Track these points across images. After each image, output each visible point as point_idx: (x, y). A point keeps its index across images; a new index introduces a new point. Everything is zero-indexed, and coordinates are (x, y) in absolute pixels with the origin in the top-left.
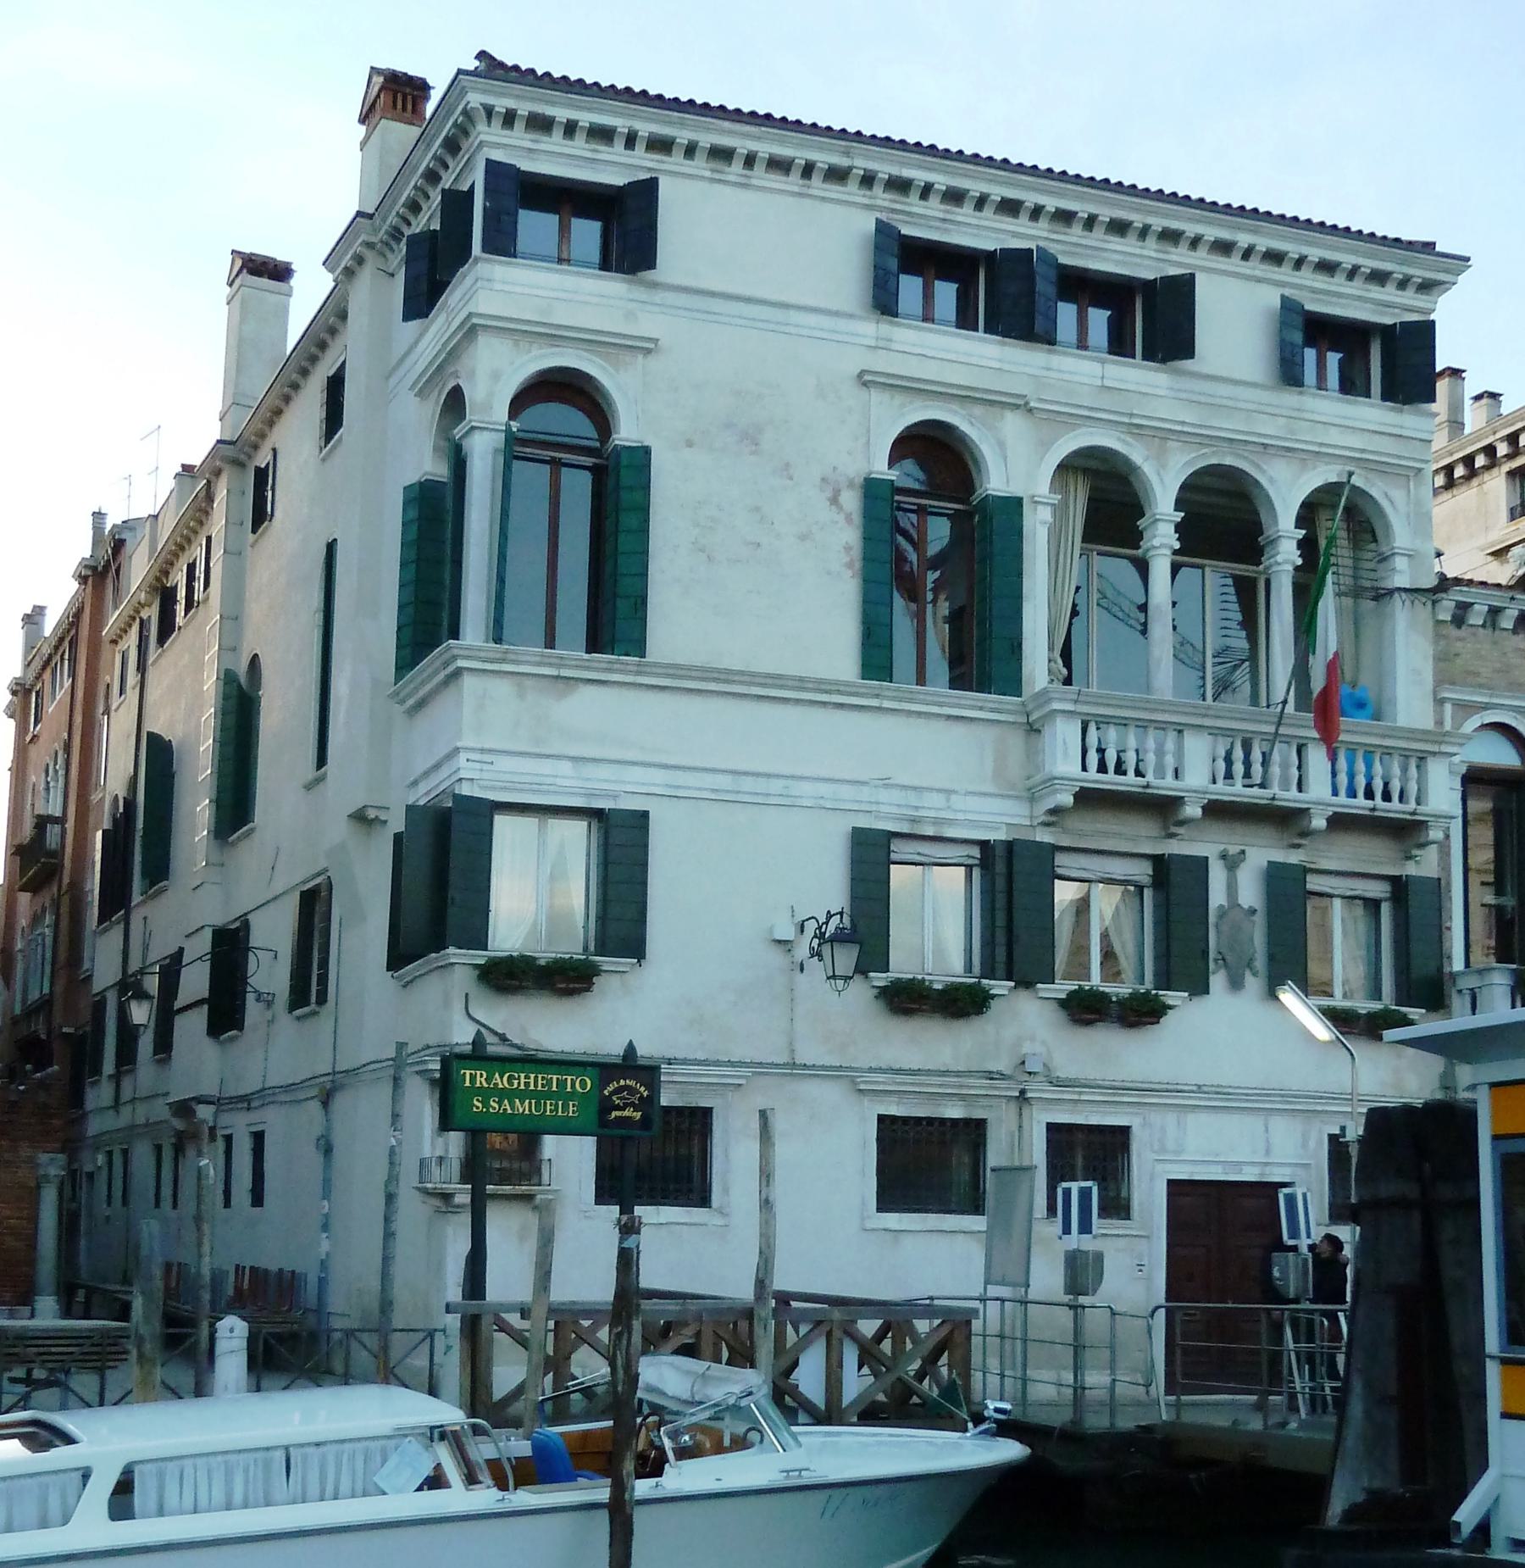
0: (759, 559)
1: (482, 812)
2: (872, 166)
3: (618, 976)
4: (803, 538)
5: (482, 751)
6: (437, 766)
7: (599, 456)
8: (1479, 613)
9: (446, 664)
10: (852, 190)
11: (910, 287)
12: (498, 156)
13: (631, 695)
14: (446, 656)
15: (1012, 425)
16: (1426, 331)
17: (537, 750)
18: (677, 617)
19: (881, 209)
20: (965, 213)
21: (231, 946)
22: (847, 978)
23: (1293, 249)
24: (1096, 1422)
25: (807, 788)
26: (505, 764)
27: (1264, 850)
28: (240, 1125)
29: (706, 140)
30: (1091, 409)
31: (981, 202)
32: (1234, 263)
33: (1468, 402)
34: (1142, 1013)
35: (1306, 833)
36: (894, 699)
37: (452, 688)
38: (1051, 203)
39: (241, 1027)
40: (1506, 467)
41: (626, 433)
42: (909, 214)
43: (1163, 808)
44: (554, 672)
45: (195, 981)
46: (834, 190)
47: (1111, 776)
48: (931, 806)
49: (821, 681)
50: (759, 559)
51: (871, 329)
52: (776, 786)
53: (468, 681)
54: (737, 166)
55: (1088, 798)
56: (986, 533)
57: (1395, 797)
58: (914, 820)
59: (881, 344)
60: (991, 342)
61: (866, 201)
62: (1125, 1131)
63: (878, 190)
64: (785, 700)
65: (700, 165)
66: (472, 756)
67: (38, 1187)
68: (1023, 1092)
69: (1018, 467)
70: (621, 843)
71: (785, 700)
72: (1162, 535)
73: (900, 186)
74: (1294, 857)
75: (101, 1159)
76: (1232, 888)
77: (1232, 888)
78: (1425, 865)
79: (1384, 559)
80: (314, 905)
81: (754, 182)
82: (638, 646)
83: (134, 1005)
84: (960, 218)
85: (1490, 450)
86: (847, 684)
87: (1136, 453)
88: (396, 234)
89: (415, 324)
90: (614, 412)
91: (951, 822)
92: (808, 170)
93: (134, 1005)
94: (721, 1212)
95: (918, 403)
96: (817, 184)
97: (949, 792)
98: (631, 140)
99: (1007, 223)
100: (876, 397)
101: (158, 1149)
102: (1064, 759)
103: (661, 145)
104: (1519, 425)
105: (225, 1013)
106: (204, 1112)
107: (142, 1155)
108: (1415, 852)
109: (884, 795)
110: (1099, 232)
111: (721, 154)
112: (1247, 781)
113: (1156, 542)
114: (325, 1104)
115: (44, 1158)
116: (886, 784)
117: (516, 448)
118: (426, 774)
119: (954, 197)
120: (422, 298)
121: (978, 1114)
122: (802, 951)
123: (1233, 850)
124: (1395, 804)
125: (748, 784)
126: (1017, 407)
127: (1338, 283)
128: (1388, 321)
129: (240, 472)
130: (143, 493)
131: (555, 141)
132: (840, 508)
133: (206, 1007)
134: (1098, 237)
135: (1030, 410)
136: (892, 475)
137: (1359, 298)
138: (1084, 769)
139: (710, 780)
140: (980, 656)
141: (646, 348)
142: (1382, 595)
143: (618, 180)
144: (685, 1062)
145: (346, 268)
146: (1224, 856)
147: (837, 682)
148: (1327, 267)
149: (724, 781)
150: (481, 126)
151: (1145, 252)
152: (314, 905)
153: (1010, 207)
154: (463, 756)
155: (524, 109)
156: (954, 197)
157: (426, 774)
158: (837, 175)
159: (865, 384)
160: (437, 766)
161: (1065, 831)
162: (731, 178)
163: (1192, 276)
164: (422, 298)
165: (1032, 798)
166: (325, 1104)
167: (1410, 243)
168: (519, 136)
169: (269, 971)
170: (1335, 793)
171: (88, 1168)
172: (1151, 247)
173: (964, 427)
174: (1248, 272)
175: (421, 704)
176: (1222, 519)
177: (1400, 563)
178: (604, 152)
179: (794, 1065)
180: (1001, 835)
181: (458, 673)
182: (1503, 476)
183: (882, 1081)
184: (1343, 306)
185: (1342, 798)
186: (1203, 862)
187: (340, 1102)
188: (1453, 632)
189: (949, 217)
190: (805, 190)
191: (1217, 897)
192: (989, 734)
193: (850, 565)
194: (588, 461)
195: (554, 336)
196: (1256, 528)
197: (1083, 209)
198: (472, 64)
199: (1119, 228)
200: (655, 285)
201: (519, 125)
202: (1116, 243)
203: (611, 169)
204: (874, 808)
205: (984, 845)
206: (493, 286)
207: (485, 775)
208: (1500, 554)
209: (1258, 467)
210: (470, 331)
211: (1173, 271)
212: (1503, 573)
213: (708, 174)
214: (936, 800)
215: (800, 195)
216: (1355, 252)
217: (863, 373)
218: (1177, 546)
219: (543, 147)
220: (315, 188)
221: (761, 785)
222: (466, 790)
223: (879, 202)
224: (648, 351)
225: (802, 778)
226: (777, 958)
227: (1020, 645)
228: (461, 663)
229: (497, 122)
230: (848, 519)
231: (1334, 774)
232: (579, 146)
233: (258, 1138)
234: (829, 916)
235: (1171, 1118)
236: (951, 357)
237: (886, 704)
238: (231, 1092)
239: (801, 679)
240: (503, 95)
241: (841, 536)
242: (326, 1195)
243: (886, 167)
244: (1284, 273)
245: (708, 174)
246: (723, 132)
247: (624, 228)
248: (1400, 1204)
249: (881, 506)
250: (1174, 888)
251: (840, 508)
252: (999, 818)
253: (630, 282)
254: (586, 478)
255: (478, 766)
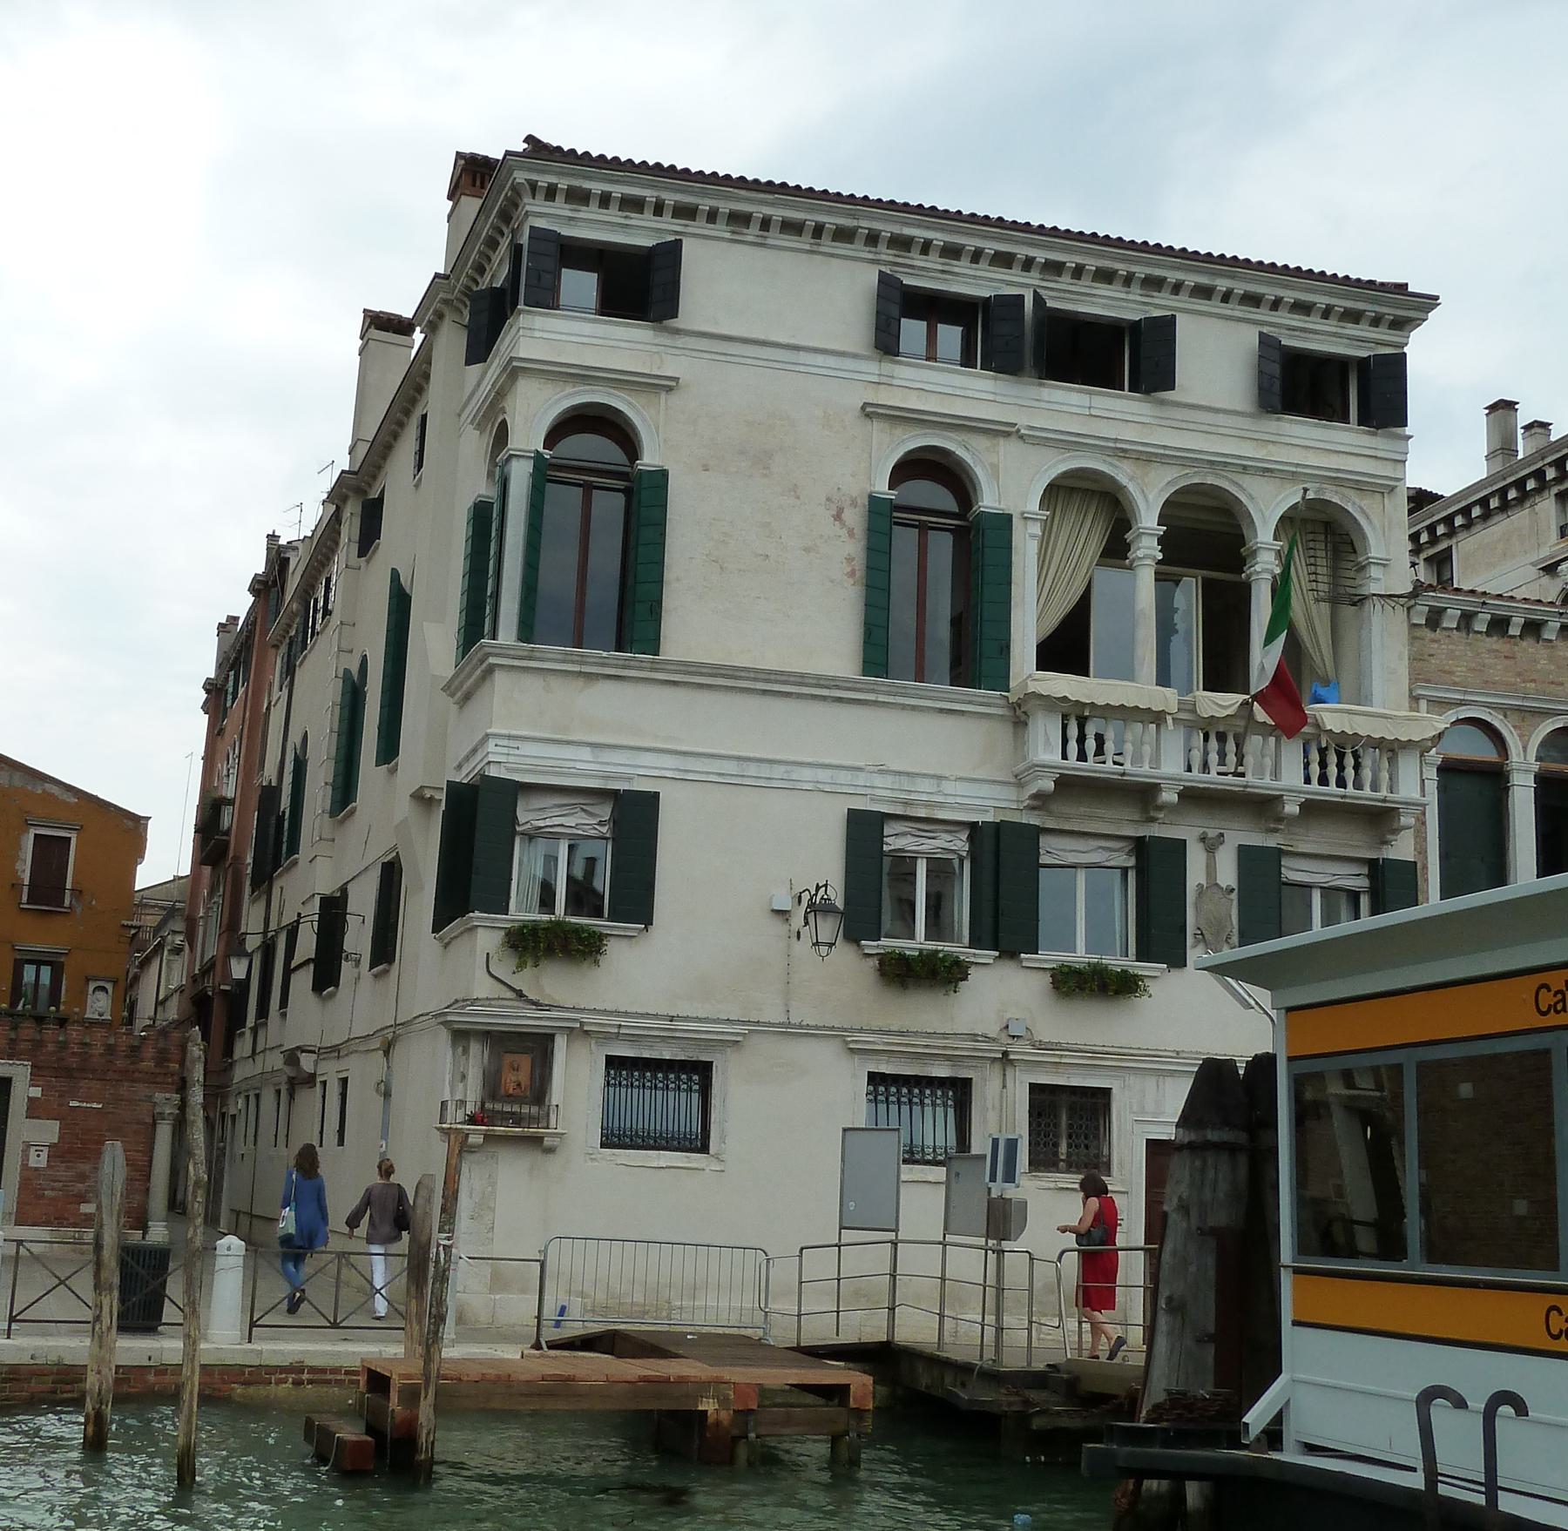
0: (767, 570)
1: (513, 791)
2: (876, 225)
3: (624, 942)
4: (807, 550)
5: (509, 737)
6: (474, 751)
7: (628, 480)
8: (1452, 617)
9: (482, 662)
10: (859, 249)
11: (913, 331)
12: (541, 223)
13: (643, 689)
14: (479, 655)
15: (1007, 451)
16: (1397, 364)
17: (565, 738)
18: (691, 623)
19: (887, 263)
20: (962, 266)
21: (333, 910)
22: (831, 945)
23: (1270, 292)
24: (1013, 1361)
25: (807, 774)
26: (529, 749)
27: (1241, 834)
28: (330, 1071)
29: (725, 207)
30: (1079, 435)
31: (977, 256)
32: (1214, 306)
33: (1520, 432)
34: (1121, 987)
35: (1280, 819)
36: (889, 694)
37: (487, 684)
38: (1041, 256)
39: (337, 985)
40: (1555, 490)
41: (649, 459)
42: (912, 267)
43: (1143, 795)
44: (577, 668)
45: (307, 944)
46: (842, 248)
49: (819, 677)
50: (767, 570)
51: (873, 368)
52: (778, 772)
53: (499, 676)
54: (754, 229)
55: (1068, 786)
56: (979, 545)
57: (1333, 781)
58: (906, 803)
59: (883, 380)
60: (986, 377)
61: (871, 256)
62: (1106, 1092)
63: (882, 247)
64: (788, 695)
65: (721, 229)
66: (500, 742)
67: (154, 1125)
68: (1005, 1054)
69: (1010, 485)
70: (634, 817)
71: (788, 695)
72: (1147, 548)
73: (902, 243)
74: (1271, 842)
75: (241, 1102)
76: (1211, 870)
77: (1211, 870)
78: (1401, 849)
79: (1362, 568)
80: (391, 874)
81: (770, 241)
82: (653, 645)
83: (233, 962)
84: (956, 270)
85: (1539, 474)
86: (847, 680)
87: (1123, 473)
88: (467, 292)
89: (476, 368)
90: (640, 441)
91: (941, 805)
92: (818, 231)
93: (233, 962)
94: (717, 1157)
95: (918, 431)
96: (827, 245)
97: (940, 778)
99: (1001, 274)
100: (877, 425)
101: (278, 1092)
102: (1046, 747)
103: (686, 212)
104: (1565, 451)
105: (326, 975)
106: (307, 1063)
107: (268, 1099)
108: (1389, 837)
109: (878, 781)
110: (1086, 281)
111: (739, 220)
112: (1222, 769)
113: (1140, 553)
114: (387, 1053)
115: (159, 1096)
117: (545, 473)
118: (467, 758)
119: (952, 252)
120: (479, 350)
121: (964, 1074)
122: (797, 920)
124: (1090, 763)
125: (752, 769)
126: (1008, 434)
127: (1314, 322)
128: (1364, 354)
129: (359, 502)
130: (299, 521)
131: (591, 212)
132: (843, 524)
133: (312, 966)
135: (1022, 437)
136: (892, 495)
137: (1335, 335)
138: (1064, 757)
139: (716, 766)
140: (973, 656)
141: (663, 386)
142: (1359, 601)
143: (648, 242)
144: (686, 1019)
145: (430, 322)
146: (1203, 839)
147: (834, 678)
148: (1302, 308)
150: (527, 199)
151: (1131, 297)
152: (391, 874)
153: (1004, 260)
154: (491, 746)
155: (563, 184)
156: (952, 252)
157: (467, 758)
158: (844, 235)
159: (868, 416)
160: (474, 751)
161: (1050, 813)
162: (750, 238)
163: (1174, 317)
164: (479, 350)
165: (1019, 782)
166: (387, 1053)
167: (1382, 284)
168: (560, 208)
169: (358, 937)
170: (1308, 781)
171: (232, 1111)
172: (1136, 294)
173: (960, 452)
174: (1229, 312)
175: (467, 697)
176: (1205, 537)
177: (1374, 572)
178: (636, 219)
179: (789, 1025)
180: (990, 817)
181: (491, 670)
182: (1553, 498)
183: (878, 1043)
184: (1322, 342)
185: (1315, 785)
187: (397, 1052)
189: (946, 268)
190: (815, 248)
191: (1195, 874)
192: (985, 725)
193: (852, 574)
194: (621, 484)
195: (583, 376)
196: (1240, 540)
197: (1071, 260)
198: (521, 147)
199: (1106, 276)
200: (677, 332)
201: (560, 198)
202: (1103, 290)
203: (641, 233)
204: (869, 791)
205: (973, 826)
206: (536, 335)
207: (511, 759)
208: (1551, 569)
209: (638, 412)
210: (514, 372)
211: (1157, 313)
212: (1550, 590)
213: (728, 235)
214: (925, 785)
215: (812, 252)
216: (1330, 294)
217: (866, 405)
218: (1160, 556)
219: (581, 215)
220: (409, 256)
221: (765, 771)
222: (493, 772)
223: (883, 257)
224: (670, 389)
225: (801, 764)
226: (779, 927)
227: (1008, 647)
228: (492, 660)
229: (540, 196)
230: (851, 533)
231: (1307, 766)
232: (613, 215)
233: (344, 1082)
234: (818, 888)
235: (1150, 1083)
236: (947, 388)
237: (881, 698)
238: (329, 1042)
239: (802, 676)
240: (543, 172)
241: (844, 549)
242: (385, 1136)
243: (887, 228)
244: (1263, 314)
245: (728, 235)
246: (739, 199)
247: (639, 286)
248: (1230, 1149)
249: (882, 518)
250: (1156, 868)
251: (843, 524)
252: (988, 801)
253: (654, 329)
254: (948, 539)
255: (505, 750)
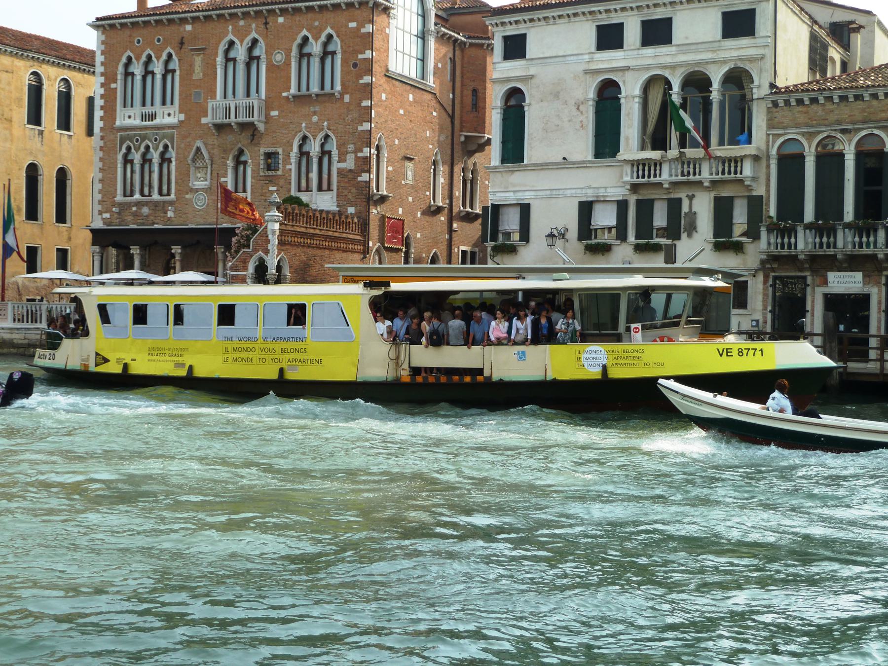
18: (533, 152)
25: (569, 192)
26: (499, 195)
47: (640, 179)
48: (602, 192)
52: (561, 192)
58: (597, 197)
97: (606, 188)
98: (511, 23)
116: (589, 187)
123: (690, 194)
125: (554, 192)
134: (652, 10)
149: (548, 193)
186: (680, 199)
188: (775, 110)
232: (514, 26)
